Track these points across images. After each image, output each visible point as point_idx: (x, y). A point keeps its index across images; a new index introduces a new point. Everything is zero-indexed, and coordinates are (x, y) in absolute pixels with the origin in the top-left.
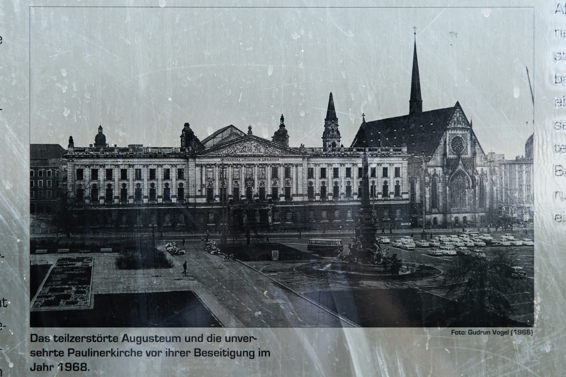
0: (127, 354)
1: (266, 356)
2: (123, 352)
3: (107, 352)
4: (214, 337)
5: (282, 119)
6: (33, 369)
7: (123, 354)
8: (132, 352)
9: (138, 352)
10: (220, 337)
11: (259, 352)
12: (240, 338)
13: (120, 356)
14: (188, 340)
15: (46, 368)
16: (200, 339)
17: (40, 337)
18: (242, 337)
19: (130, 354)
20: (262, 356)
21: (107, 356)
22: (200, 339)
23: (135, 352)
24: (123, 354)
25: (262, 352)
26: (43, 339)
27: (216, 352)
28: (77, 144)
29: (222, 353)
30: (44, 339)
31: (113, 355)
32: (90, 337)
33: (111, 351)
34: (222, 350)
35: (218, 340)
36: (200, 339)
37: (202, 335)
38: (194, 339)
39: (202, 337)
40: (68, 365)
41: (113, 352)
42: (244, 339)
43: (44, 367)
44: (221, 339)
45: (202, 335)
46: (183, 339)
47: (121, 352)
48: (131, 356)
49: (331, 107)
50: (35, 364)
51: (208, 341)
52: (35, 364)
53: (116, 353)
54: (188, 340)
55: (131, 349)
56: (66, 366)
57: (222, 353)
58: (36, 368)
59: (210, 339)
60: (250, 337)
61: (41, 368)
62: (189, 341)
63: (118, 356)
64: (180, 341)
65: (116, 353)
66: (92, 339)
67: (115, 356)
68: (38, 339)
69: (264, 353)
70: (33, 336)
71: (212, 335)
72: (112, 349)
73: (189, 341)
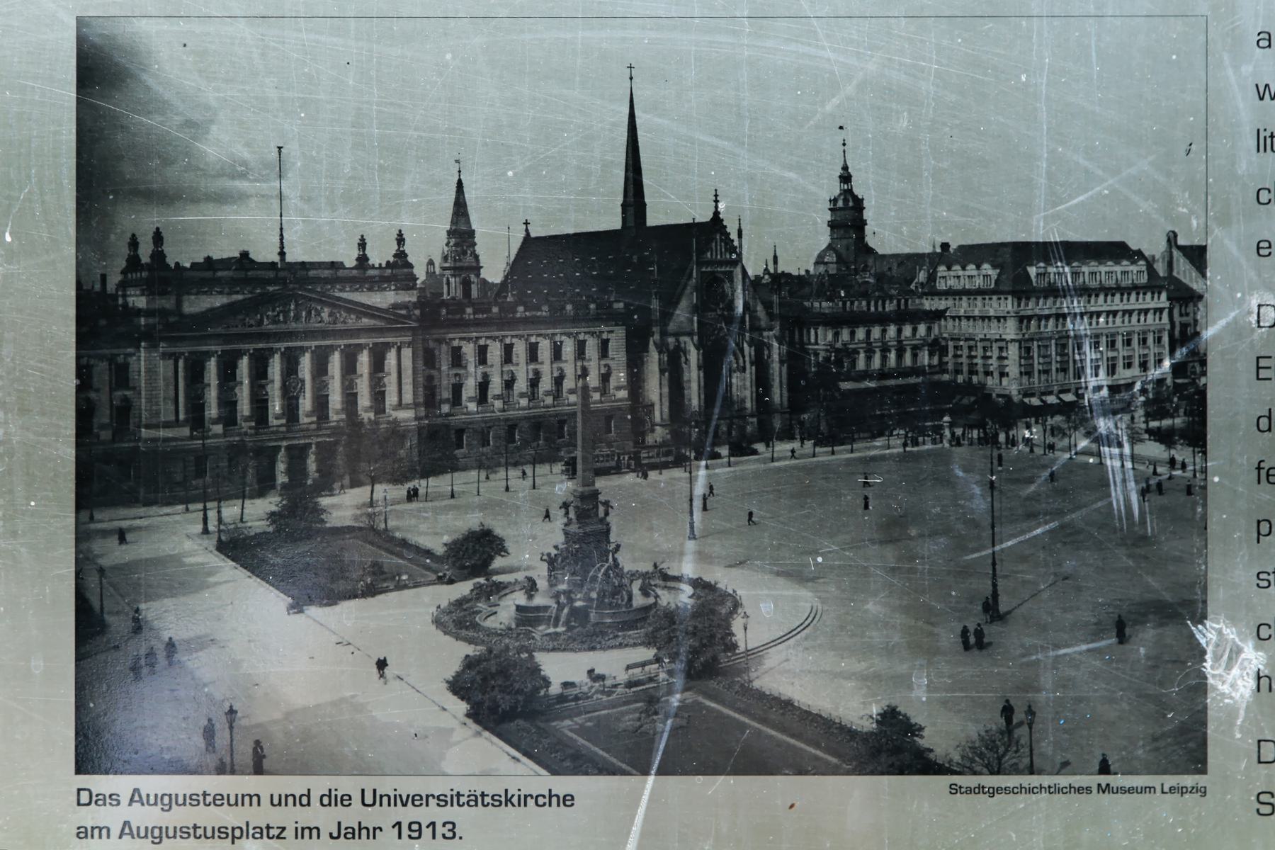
0: (541, 800)
1: (311, 837)
2: (531, 796)
3: (427, 796)
4: (336, 796)
5: (401, 240)
6: (335, 835)
7: (531, 802)
8: (551, 797)
9: (565, 796)
10: (349, 796)
11: (296, 828)
12: (404, 800)
13: (525, 805)
14: (276, 801)
15: (364, 832)
16: (305, 800)
17: (97, 795)
18: (408, 796)
19: (547, 800)
20: (303, 837)
21: (427, 805)
22: (303, 800)
23: (558, 796)
24: (531, 802)
25: (303, 829)
26: (105, 799)
27: (345, 798)
28: (289, 259)
29: (455, 799)
30: (108, 801)
31: (509, 804)
32: (198, 795)
33: (547, 794)
34: (454, 793)
35: (345, 803)
36: (305, 800)
37: (309, 790)
38: (290, 799)
39: (309, 796)
40: (415, 827)
41: (509, 796)
42: (413, 800)
43: (360, 829)
44: (350, 799)
45: (309, 790)
46: (265, 800)
47: (526, 797)
48: (550, 805)
49: (460, 208)
50: (339, 823)
51: (322, 804)
52: (339, 823)
53: (515, 800)
54: (276, 801)
55: (550, 791)
56: (410, 829)
57: (455, 799)
58: (343, 832)
59: (326, 800)
60: (427, 796)
61: (353, 834)
62: (280, 804)
63: (519, 805)
64: (259, 805)
65: (515, 800)
66: (201, 798)
67: (513, 805)
68: (94, 798)
69: (307, 832)
70: (82, 792)
71: (330, 790)
72: (506, 791)
73: (280, 804)
